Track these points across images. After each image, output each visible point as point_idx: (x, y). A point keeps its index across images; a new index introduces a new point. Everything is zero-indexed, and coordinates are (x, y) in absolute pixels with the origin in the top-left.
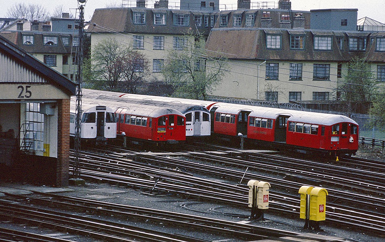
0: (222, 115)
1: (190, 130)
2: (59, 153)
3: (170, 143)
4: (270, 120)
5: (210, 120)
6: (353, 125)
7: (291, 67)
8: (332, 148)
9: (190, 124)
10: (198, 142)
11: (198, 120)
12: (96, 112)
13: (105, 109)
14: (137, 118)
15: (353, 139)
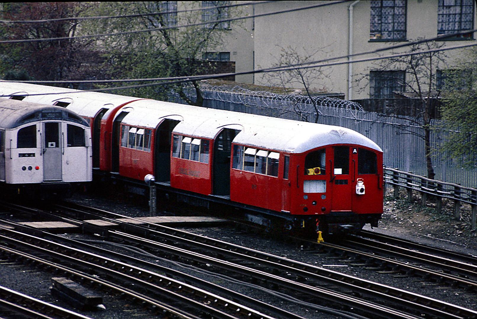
0: (133, 130)
1: (34, 169)
2: (364, 230)
4: (147, 130)
5: (89, 142)
6: (364, 151)
7: (443, 6)
8: (306, 209)
9: (34, 155)
10: (51, 197)
11: (54, 143)
15: (364, 188)
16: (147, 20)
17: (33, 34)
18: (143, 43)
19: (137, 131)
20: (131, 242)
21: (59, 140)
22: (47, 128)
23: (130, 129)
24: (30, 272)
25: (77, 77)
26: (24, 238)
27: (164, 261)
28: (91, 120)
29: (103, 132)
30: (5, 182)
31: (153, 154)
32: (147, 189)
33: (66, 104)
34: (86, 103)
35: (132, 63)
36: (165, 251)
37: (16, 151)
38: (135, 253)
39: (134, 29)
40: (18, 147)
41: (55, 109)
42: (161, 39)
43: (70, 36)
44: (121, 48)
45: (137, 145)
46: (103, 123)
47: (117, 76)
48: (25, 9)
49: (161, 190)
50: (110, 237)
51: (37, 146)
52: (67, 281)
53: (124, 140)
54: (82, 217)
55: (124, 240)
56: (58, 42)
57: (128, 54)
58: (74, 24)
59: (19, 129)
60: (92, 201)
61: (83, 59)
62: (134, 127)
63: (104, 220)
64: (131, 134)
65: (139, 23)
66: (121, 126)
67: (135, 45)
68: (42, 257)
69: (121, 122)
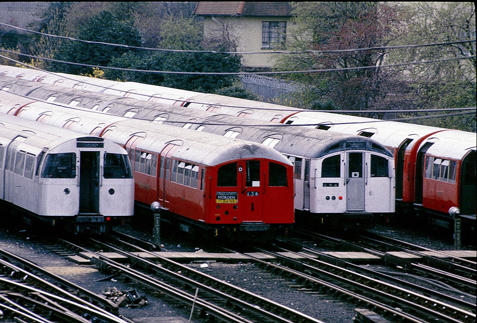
0: (438, 162)
3: (247, 229)
4: (453, 162)
5: (392, 172)
10: (353, 228)
11: (358, 173)
12: (77, 151)
13: (101, 146)
14: (186, 168)
16: (457, 50)
17: (341, 65)
18: (451, 72)
19: (442, 162)
20: (434, 276)
21: (363, 170)
22: (349, 159)
23: (435, 160)
24: (334, 302)
25: (381, 107)
26: (328, 268)
27: (469, 297)
28: (395, 150)
29: (407, 162)
30: (309, 211)
31: (458, 187)
32: (452, 222)
33: (370, 134)
34: (391, 134)
35: (439, 93)
36: (470, 287)
37: (320, 181)
38: (439, 287)
39: (443, 58)
40: (322, 177)
41: (359, 139)
42: (470, 68)
43: (377, 65)
44: (428, 77)
45: (442, 176)
46: (407, 154)
47: (423, 107)
48: (334, 40)
49: (466, 223)
50: (413, 270)
51: (341, 176)
52: (370, 312)
53: (428, 171)
54: (384, 249)
55: (427, 274)
56: (365, 72)
57: (435, 84)
58: (381, 54)
59: (323, 159)
60: (395, 232)
61: (389, 89)
62: (439, 158)
63: (407, 252)
64: (436, 165)
65: (448, 52)
66: (425, 157)
67: (443, 75)
68: (345, 288)
69: (425, 153)
